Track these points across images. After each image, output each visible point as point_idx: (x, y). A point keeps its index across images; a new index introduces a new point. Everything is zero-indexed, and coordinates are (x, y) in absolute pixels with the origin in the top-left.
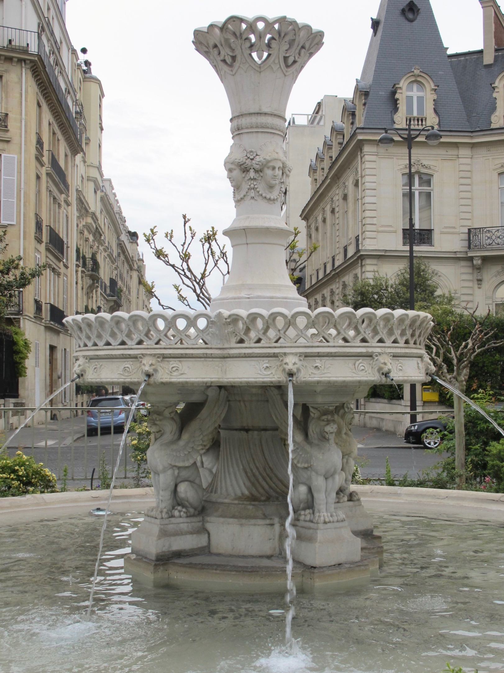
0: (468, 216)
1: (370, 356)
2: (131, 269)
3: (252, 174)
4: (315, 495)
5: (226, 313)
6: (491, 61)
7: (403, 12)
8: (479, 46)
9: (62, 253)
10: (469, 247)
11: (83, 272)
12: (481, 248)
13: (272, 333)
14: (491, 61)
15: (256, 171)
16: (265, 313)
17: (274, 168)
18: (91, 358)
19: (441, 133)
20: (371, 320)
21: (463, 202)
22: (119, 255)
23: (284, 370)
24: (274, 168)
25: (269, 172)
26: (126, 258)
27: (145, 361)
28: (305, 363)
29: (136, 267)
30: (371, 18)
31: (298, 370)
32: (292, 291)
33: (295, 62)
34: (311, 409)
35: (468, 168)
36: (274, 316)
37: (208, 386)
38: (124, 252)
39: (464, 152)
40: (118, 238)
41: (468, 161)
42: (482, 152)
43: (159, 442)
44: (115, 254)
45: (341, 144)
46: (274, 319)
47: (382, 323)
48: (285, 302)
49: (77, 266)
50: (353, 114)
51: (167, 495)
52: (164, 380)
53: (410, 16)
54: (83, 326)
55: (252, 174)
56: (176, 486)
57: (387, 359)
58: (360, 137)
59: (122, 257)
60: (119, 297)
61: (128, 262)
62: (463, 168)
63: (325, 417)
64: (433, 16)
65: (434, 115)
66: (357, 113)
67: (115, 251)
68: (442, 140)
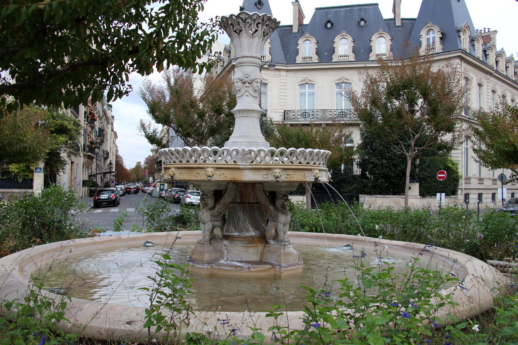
0: (284, 104)
1: (310, 170)
2: (108, 123)
3: (247, 84)
4: (279, 233)
5: (247, 149)
6: (296, 31)
7: (256, 4)
8: (291, 24)
9: (78, 114)
10: (284, 119)
11: (87, 124)
12: (290, 120)
13: (258, 159)
14: (296, 31)
15: (249, 83)
16: (256, 149)
17: (257, 82)
18: (178, 168)
19: (276, 64)
20: (303, 153)
21: (282, 97)
22: (103, 116)
23: (274, 176)
24: (257, 82)
25: (254, 84)
26: (106, 117)
27: (208, 170)
28: (283, 173)
29: (110, 122)
30: (512, 55)
31: (213, 175)
32: (261, 138)
33: (267, 34)
34: (278, 194)
35: (284, 81)
36: (259, 151)
37: (228, 182)
38: (105, 115)
39: (283, 73)
40: (103, 107)
41: (285, 78)
42: (291, 74)
43: (205, 208)
44: (101, 115)
45: (223, 66)
46: (260, 152)
47: (308, 155)
48: (256, 144)
49: (85, 121)
50: (230, 52)
51: (208, 233)
52: (217, 179)
53: (259, 6)
54: (175, 153)
55: (247, 84)
56: (213, 229)
57: (317, 171)
58: (234, 63)
59: (104, 117)
60: (103, 138)
61: (107, 120)
62: (282, 81)
63: (284, 198)
64: (269, 8)
65: (269, 55)
66: (232, 51)
67: (101, 114)
68: (276, 67)
